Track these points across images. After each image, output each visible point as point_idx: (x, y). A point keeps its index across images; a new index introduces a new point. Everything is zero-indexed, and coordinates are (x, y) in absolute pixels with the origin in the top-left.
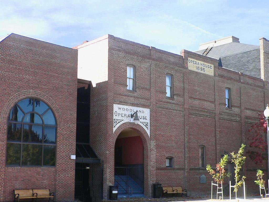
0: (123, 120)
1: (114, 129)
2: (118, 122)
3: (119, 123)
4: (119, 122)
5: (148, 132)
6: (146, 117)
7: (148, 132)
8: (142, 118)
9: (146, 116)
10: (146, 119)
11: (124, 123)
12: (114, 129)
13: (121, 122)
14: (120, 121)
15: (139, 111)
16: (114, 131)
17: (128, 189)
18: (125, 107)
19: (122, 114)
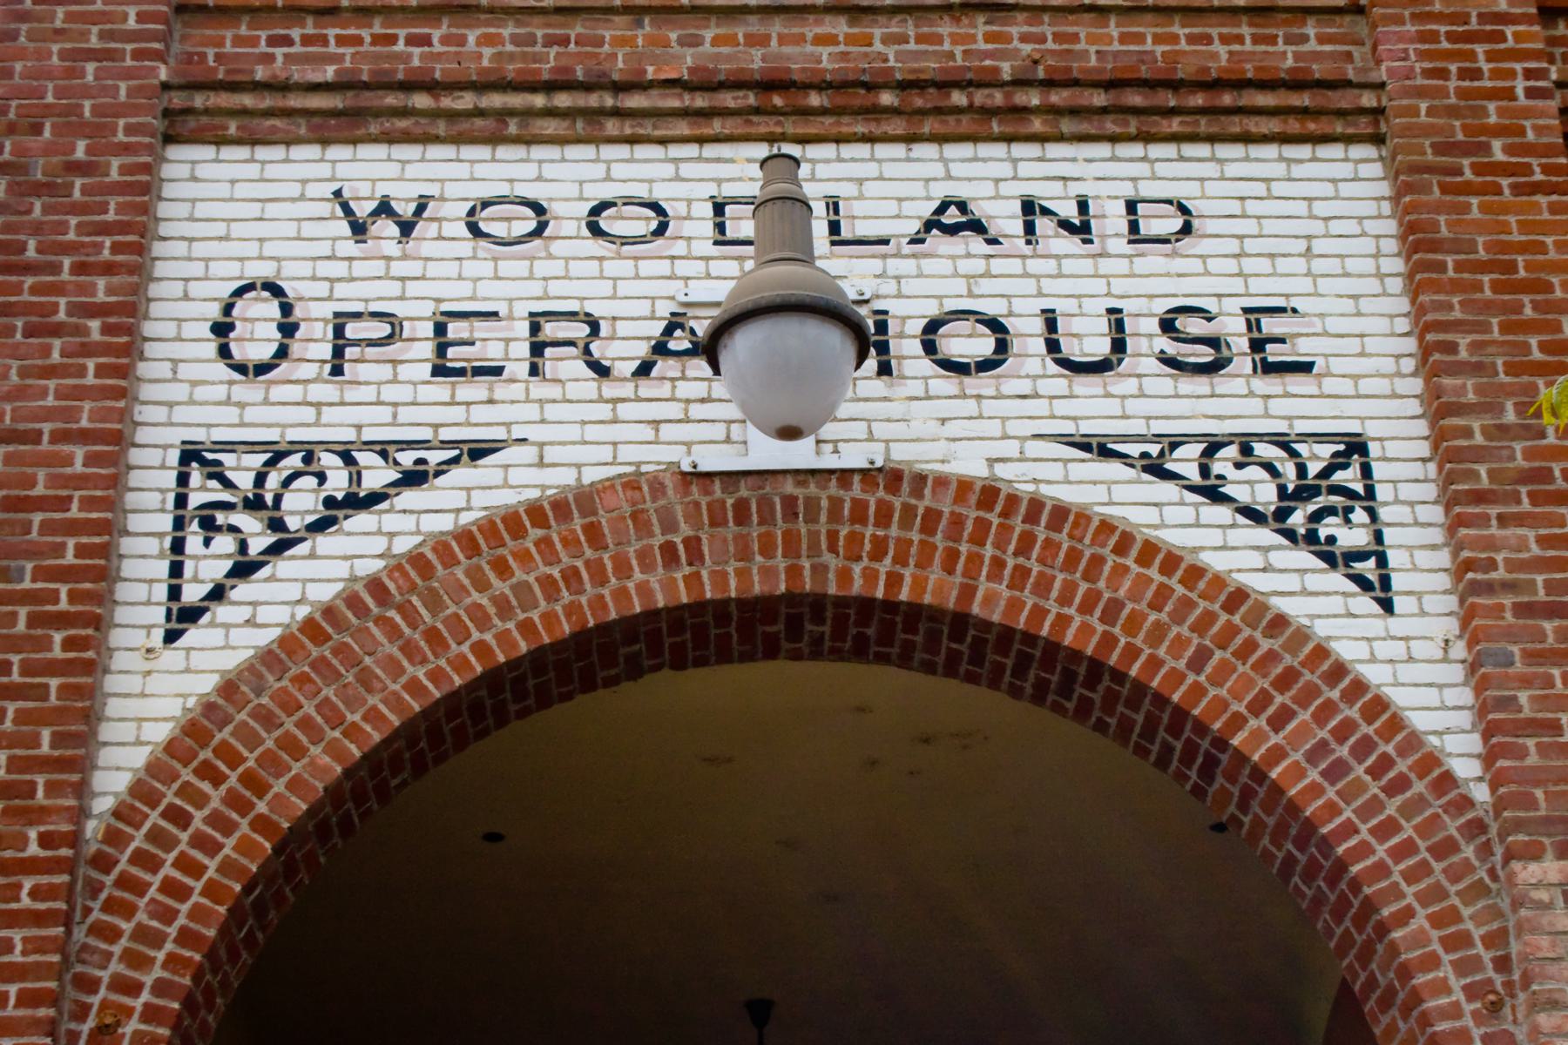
0: (478, 452)
1: (153, 692)
2: (301, 503)
3: (362, 520)
4: (357, 502)
5: (1410, 657)
6: (1270, 326)
7: (1410, 657)
8: (1146, 339)
9: (1265, 291)
10: (1269, 368)
11: (512, 522)
12: (153, 692)
13: (409, 498)
14: (377, 476)
15: (1028, 207)
16: (139, 758)
17: (722, 86)
18: (569, 175)
19: (1253, 314)
